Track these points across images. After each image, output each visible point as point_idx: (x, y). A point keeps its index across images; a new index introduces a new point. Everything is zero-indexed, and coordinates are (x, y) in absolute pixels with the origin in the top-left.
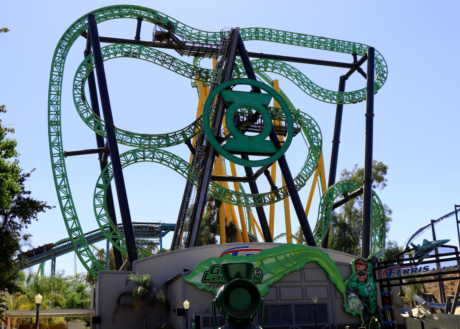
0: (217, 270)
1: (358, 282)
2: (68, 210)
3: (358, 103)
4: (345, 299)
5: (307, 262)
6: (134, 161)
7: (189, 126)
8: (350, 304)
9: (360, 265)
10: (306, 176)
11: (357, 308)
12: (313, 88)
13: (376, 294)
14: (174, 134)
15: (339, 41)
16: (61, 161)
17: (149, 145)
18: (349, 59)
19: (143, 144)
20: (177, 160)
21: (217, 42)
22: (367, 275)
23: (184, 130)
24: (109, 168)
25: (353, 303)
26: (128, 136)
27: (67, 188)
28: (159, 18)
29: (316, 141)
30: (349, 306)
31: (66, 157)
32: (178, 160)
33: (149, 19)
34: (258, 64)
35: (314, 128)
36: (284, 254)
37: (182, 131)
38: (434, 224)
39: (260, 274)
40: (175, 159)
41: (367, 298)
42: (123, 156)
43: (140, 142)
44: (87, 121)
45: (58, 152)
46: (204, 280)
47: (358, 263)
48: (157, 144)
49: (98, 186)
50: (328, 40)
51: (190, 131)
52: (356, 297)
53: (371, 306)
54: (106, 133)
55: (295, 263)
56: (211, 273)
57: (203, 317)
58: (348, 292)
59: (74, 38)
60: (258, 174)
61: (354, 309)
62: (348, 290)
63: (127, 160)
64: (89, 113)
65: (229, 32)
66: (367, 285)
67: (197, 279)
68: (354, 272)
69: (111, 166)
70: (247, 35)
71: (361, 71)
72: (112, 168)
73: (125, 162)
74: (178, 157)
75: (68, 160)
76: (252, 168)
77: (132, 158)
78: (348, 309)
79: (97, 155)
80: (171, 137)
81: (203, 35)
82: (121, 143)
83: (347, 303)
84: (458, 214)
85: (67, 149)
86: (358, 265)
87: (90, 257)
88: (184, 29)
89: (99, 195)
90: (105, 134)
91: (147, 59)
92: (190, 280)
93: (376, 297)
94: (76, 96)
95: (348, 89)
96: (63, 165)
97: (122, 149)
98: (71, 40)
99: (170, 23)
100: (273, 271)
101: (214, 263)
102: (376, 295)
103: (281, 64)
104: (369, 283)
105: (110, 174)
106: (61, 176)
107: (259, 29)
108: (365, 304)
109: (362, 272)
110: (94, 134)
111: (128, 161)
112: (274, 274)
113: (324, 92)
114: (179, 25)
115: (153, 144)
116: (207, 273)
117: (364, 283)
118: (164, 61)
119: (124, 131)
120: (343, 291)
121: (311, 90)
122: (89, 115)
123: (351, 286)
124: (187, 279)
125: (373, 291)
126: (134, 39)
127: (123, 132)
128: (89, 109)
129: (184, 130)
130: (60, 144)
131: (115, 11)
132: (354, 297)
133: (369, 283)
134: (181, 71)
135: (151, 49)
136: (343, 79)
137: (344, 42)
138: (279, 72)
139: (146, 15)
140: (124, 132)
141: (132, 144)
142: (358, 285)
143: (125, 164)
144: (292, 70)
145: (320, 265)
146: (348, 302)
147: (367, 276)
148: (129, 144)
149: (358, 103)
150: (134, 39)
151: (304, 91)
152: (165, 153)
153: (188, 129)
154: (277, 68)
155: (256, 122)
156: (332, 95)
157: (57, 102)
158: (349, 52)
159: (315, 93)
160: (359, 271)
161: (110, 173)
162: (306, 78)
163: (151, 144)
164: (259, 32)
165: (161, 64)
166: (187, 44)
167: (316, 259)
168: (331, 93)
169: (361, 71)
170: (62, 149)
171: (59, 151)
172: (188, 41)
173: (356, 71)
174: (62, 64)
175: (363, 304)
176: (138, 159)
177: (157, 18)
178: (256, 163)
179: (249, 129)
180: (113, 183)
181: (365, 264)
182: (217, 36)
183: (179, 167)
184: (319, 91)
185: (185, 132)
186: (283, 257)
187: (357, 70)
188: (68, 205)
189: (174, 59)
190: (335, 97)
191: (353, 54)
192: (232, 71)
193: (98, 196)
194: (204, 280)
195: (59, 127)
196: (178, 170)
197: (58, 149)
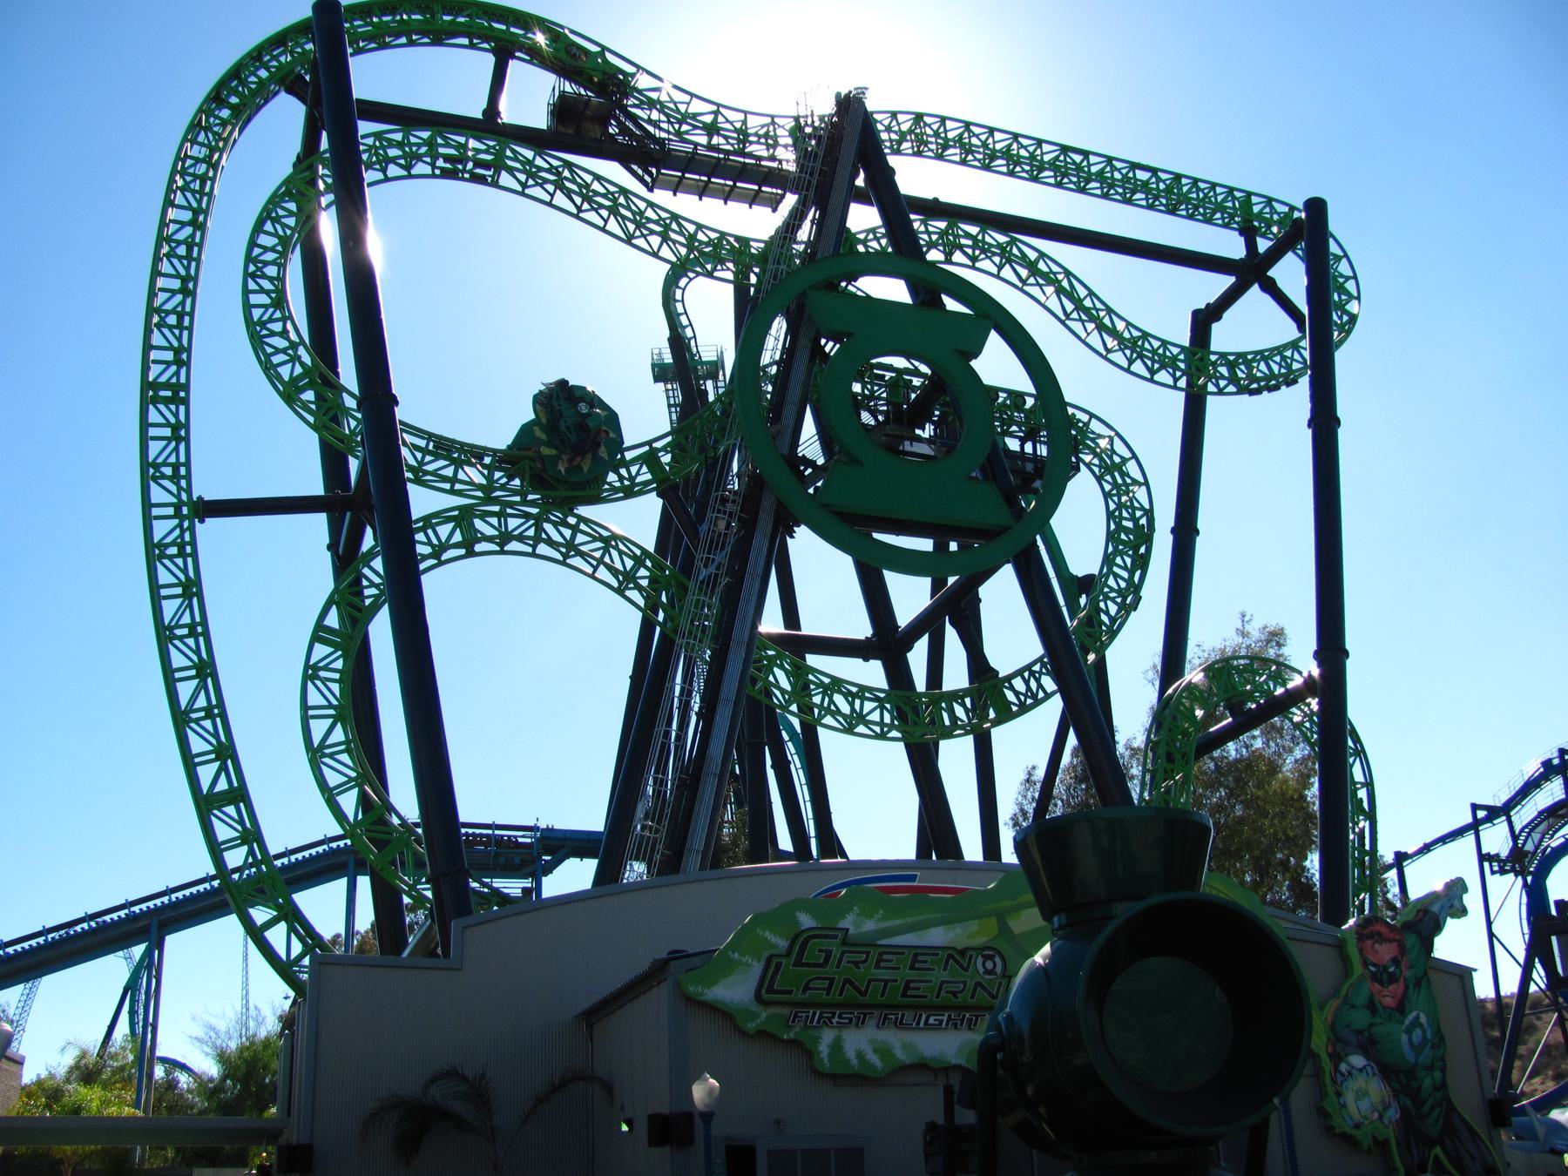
0: (820, 951)
1: (1372, 1006)
2: (202, 723)
3: (1283, 388)
4: (1327, 1078)
8: (1349, 1098)
9: (1377, 942)
11: (1376, 1115)
13: (1443, 1059)
15: (1195, 181)
16: (182, 536)
18: (1231, 245)
22: (1405, 980)
24: (366, 571)
25: (1361, 1094)
27: (218, 720)
28: (574, 51)
30: (1344, 1106)
31: (202, 521)
33: (535, 56)
37: (647, 448)
38: (1405, 864)
39: (999, 969)
40: (621, 553)
41: (1411, 1072)
42: (424, 529)
44: (290, 394)
46: (767, 992)
47: (1371, 935)
49: (320, 633)
52: (1368, 1069)
53: (1428, 1105)
56: (798, 963)
57: (769, 1151)
58: (1339, 1047)
59: (263, 95)
61: (1365, 1118)
62: (1339, 1040)
63: (435, 541)
66: (1407, 1022)
67: (735, 990)
69: (378, 564)
71: (1271, 288)
75: (210, 531)
77: (458, 537)
78: (1343, 1117)
79: (320, 520)
82: (418, 481)
83: (1339, 1094)
84: (1481, 833)
85: (207, 487)
86: (1370, 942)
91: (523, 190)
92: (706, 991)
93: (1443, 1069)
96: (187, 549)
97: (422, 501)
98: (246, 101)
99: (611, 74)
101: (806, 921)
102: (1442, 1063)
104: (1414, 1014)
106: (213, 756)
107: (925, 119)
108: (1402, 1097)
109: (1385, 968)
110: (312, 440)
116: (778, 965)
117: (1397, 1014)
119: (430, 436)
123: (1348, 1026)
124: (691, 989)
125: (1432, 1047)
126: (480, 116)
127: (423, 438)
130: (181, 473)
132: (1361, 1070)
133: (1414, 1014)
136: (1204, 320)
137: (1213, 186)
140: (429, 440)
141: (458, 486)
146: (1339, 1089)
147: (1407, 987)
148: (447, 486)
149: (1283, 388)
150: (480, 116)
152: (583, 527)
154: (419, 158)
158: (1229, 223)
160: (1375, 965)
161: (367, 587)
162: (1091, 294)
165: (575, 211)
169: (1271, 288)
170: (189, 490)
171: (178, 496)
173: (1256, 287)
174: (196, 249)
175: (1396, 1097)
176: (479, 541)
177: (568, 52)
180: (381, 632)
181: (1397, 937)
191: (1242, 232)
193: (322, 674)
194: (767, 992)
195: (182, 408)
196: (628, 593)
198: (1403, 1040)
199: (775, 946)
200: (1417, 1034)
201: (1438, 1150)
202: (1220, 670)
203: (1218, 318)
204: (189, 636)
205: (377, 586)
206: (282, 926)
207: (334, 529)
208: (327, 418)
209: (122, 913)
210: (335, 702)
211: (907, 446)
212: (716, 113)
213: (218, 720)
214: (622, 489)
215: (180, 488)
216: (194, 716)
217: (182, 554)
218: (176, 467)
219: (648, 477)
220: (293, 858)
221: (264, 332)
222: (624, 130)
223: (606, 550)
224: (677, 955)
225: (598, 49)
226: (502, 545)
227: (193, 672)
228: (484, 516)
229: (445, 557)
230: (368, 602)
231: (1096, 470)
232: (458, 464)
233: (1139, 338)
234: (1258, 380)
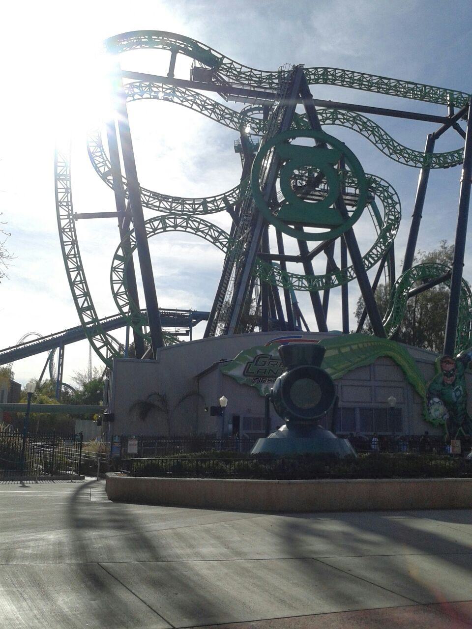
1: (443, 384)
3: (458, 165)
5: (380, 357)
6: (162, 230)
7: (233, 190)
8: (432, 411)
10: (377, 255)
12: (395, 147)
13: (466, 401)
14: (214, 199)
16: (70, 225)
17: (175, 218)
19: (174, 210)
20: (216, 231)
21: (273, 85)
23: (227, 194)
24: (131, 237)
26: (155, 199)
27: (84, 284)
29: (393, 213)
30: (430, 413)
31: (77, 220)
32: (218, 231)
33: (187, 53)
34: (324, 115)
35: (391, 198)
36: (349, 345)
40: (214, 230)
42: (149, 223)
43: (171, 206)
44: (104, 177)
45: (67, 213)
46: (247, 372)
47: (445, 362)
48: (192, 210)
49: (116, 257)
50: (419, 86)
51: (233, 197)
54: (128, 193)
55: (363, 357)
56: (256, 364)
60: (317, 251)
63: (153, 228)
64: (107, 166)
65: (289, 72)
66: (455, 389)
67: (237, 372)
68: (440, 371)
69: (134, 234)
70: (312, 77)
72: (135, 236)
73: (151, 230)
74: (218, 228)
75: (80, 224)
76: (308, 242)
77: (161, 226)
80: (210, 202)
81: (256, 75)
82: (147, 207)
83: (429, 410)
85: (78, 209)
87: (104, 342)
88: (231, 66)
89: (117, 268)
90: (127, 194)
94: (59, 191)
95: (436, 150)
96: (73, 230)
100: (334, 366)
101: (259, 352)
103: (354, 115)
104: (458, 386)
105: (132, 243)
106: (76, 269)
110: (112, 193)
111: (156, 229)
112: (336, 369)
113: (407, 153)
114: (225, 61)
115: (187, 210)
118: (204, 106)
119: (151, 192)
120: (423, 394)
121: (391, 149)
122: (107, 169)
128: (107, 162)
129: (227, 194)
130: (69, 204)
131: (143, 38)
133: (458, 386)
134: (226, 120)
135: (188, 90)
136: (433, 138)
138: (351, 126)
139: (183, 46)
141: (160, 209)
142: (443, 388)
143: (151, 232)
144: (368, 123)
145: (394, 361)
147: (456, 378)
148: (157, 209)
149: (458, 165)
151: (382, 151)
152: (202, 222)
153: (232, 194)
155: (318, 187)
156: (418, 157)
157: (70, 229)
159: (396, 153)
162: (386, 134)
163: (185, 210)
164: (329, 74)
165: (200, 110)
166: (234, 86)
167: (391, 354)
168: (417, 153)
170: (72, 210)
171: (68, 212)
172: (236, 82)
176: (168, 227)
178: (314, 237)
179: (308, 197)
180: (135, 254)
182: (273, 77)
183: (218, 239)
184: (401, 150)
185: (228, 197)
186: (347, 349)
187: (452, 127)
188: (78, 279)
189: (217, 104)
190: (422, 160)
192: (291, 124)
193: (117, 270)
195: (68, 182)
196: (216, 244)
197: (67, 210)
198: (453, 395)
199: (249, 360)
200: (458, 393)
201: (461, 428)
202: (422, 267)
203: (438, 138)
204: (69, 231)
205: (135, 242)
206: (105, 348)
207: (120, 221)
208: (117, 187)
209: (50, 338)
210: (122, 279)
211: (272, 230)
212: (251, 72)
213: (84, 284)
214: (215, 209)
215: (69, 209)
216: (70, 256)
217: (70, 231)
218: (67, 202)
219: (224, 205)
220: (108, 320)
221: (94, 156)
222: (217, 80)
223: (209, 230)
224: (222, 361)
225: (208, 49)
226: (175, 228)
227: (70, 243)
228: (168, 218)
229: (156, 232)
230: (132, 246)
231: (382, 198)
232: (160, 201)
233: (403, 149)
234: (448, 163)
